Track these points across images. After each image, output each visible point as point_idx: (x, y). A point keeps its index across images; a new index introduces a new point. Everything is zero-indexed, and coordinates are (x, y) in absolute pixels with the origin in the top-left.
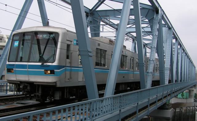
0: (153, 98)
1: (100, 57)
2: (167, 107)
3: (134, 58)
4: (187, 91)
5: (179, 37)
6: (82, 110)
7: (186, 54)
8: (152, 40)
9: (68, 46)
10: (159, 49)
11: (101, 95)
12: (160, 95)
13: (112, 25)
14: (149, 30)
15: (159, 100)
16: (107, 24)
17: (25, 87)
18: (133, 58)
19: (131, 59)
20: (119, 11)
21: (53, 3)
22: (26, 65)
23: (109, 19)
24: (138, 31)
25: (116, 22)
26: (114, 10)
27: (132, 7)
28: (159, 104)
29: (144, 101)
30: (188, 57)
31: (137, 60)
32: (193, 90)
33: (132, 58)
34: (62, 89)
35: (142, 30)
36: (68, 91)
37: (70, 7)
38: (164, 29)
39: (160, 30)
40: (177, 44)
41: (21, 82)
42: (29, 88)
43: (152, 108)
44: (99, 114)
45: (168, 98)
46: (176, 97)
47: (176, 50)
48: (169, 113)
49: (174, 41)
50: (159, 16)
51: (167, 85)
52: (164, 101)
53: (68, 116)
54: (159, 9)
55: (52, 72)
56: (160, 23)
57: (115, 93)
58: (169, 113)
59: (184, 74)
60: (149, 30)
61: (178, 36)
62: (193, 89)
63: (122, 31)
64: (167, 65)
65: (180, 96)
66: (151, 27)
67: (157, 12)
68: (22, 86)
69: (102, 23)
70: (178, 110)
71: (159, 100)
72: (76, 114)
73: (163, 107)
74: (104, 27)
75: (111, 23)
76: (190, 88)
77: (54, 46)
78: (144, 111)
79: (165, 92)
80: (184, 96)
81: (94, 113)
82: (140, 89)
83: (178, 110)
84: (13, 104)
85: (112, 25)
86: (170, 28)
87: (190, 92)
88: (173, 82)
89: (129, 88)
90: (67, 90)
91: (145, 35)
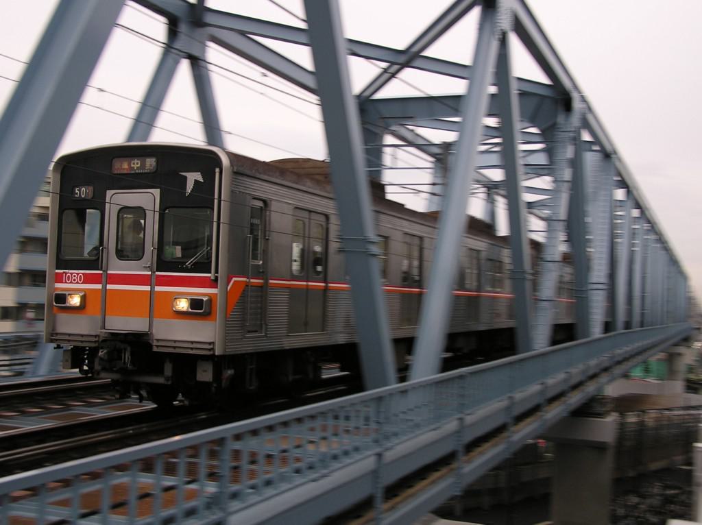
0: (555, 380)
1: (222, 202)
2: (599, 409)
4: (662, 355)
8: (554, 192)
10: (575, 226)
12: (577, 371)
13: (425, 148)
14: (541, 159)
15: (575, 387)
16: (410, 144)
17: (115, 355)
20: (452, 104)
25: (437, 136)
27: (493, 90)
28: (575, 399)
29: (529, 392)
32: (680, 354)
35: (521, 162)
37: (314, 98)
38: (591, 159)
42: (127, 356)
43: (554, 412)
45: (604, 378)
46: (626, 376)
48: (606, 428)
50: (575, 120)
51: (599, 340)
52: (591, 388)
54: (575, 95)
56: (576, 140)
58: (606, 428)
60: (541, 159)
62: (682, 349)
63: (463, 167)
64: (598, 273)
65: (637, 373)
66: (549, 151)
68: (105, 351)
70: (632, 419)
71: (575, 387)
72: (203, 471)
73: (587, 410)
79: (593, 362)
81: (388, 428)
83: (632, 419)
86: (608, 155)
87: (671, 358)
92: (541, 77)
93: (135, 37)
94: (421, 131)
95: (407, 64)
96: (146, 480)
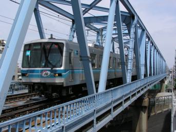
7: (159, 53)
9: (70, 54)
14: (127, 32)
16: (92, 29)
17: (39, 87)
21: (49, 16)
22: (38, 70)
25: (99, 26)
26: (95, 17)
31: (119, 60)
34: (67, 87)
39: (136, 33)
41: (35, 83)
42: (42, 88)
50: (135, 21)
53: (26, 128)
54: (135, 15)
55: (60, 75)
57: (107, 89)
60: (127, 32)
61: (133, 10)
64: (142, 61)
67: (133, 17)
77: (60, 54)
82: (87, 95)
88: (126, 83)
89: (80, 95)
91: (124, 36)
92: (125, 10)
93: (150, 33)
94: (94, 26)
95: (91, 8)
96: (43, 119)
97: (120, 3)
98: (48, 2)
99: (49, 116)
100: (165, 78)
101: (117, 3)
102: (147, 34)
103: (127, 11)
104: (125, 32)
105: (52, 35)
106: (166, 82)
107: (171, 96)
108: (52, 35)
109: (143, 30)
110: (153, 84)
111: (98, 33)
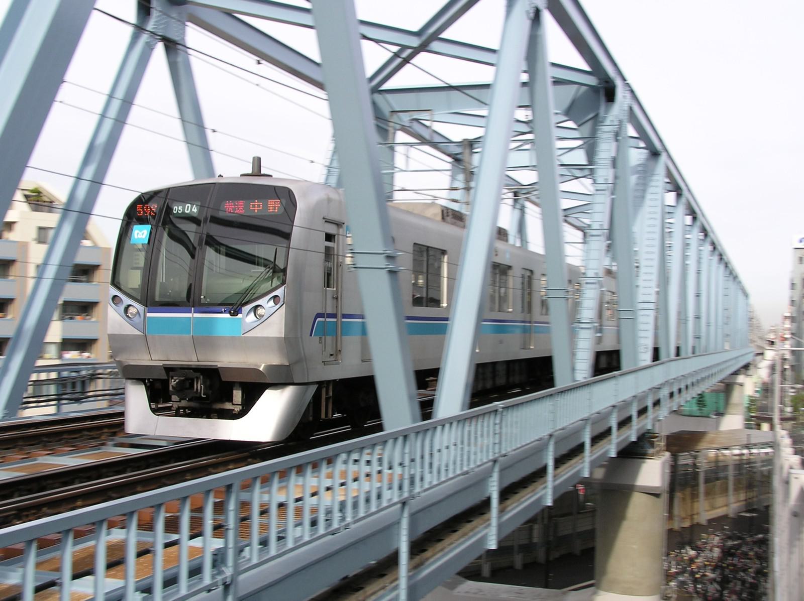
3: (531, 271)
5: (687, 185)
6: (368, 462)
11: (426, 408)
14: (580, 157)
16: (424, 141)
17: (185, 388)
18: (528, 273)
19: (523, 277)
23: (427, 123)
24: (542, 165)
25: (457, 132)
30: (721, 255)
32: (741, 385)
33: (528, 273)
36: (331, 394)
40: (681, 210)
42: (199, 386)
44: (672, 395)
47: (677, 230)
49: (671, 198)
54: (619, 83)
59: (708, 324)
67: (610, 94)
69: (401, 137)
74: (413, 152)
75: (437, 139)
76: (120, 403)
78: (566, 468)
80: (704, 406)
84: (104, 449)
85: (437, 143)
88: (552, 386)
90: (327, 393)
91: (565, 179)
94: (437, 127)
95: (424, 48)
97: (548, 19)
98: (229, 13)
99: (147, 526)
100: (746, 367)
101: (536, 18)
102: (669, 174)
103: (586, 67)
104: (569, 159)
105: (257, 162)
106: (748, 386)
107: (774, 445)
108: (257, 162)
109: (655, 154)
110: (694, 392)
111: (457, 160)
